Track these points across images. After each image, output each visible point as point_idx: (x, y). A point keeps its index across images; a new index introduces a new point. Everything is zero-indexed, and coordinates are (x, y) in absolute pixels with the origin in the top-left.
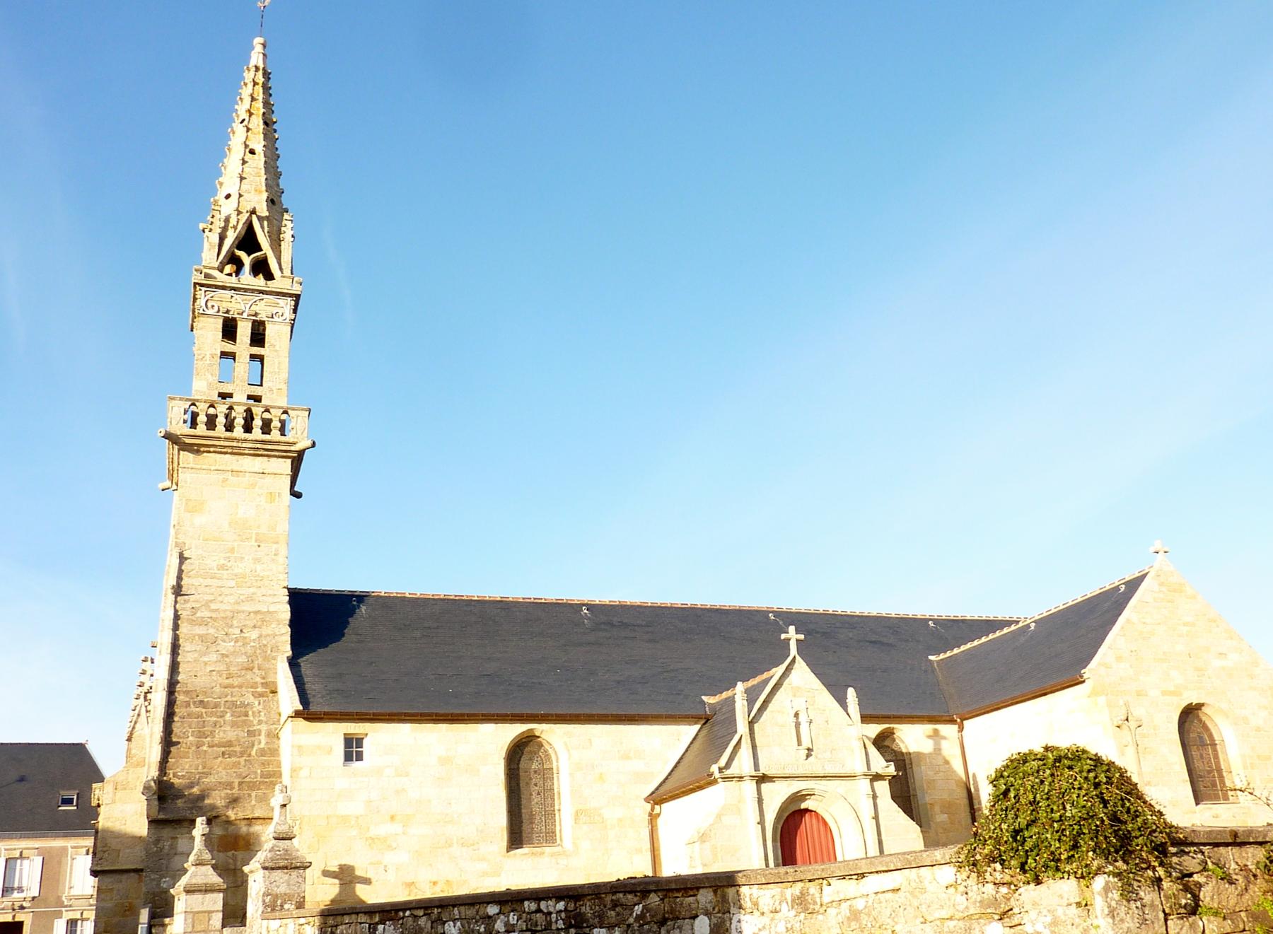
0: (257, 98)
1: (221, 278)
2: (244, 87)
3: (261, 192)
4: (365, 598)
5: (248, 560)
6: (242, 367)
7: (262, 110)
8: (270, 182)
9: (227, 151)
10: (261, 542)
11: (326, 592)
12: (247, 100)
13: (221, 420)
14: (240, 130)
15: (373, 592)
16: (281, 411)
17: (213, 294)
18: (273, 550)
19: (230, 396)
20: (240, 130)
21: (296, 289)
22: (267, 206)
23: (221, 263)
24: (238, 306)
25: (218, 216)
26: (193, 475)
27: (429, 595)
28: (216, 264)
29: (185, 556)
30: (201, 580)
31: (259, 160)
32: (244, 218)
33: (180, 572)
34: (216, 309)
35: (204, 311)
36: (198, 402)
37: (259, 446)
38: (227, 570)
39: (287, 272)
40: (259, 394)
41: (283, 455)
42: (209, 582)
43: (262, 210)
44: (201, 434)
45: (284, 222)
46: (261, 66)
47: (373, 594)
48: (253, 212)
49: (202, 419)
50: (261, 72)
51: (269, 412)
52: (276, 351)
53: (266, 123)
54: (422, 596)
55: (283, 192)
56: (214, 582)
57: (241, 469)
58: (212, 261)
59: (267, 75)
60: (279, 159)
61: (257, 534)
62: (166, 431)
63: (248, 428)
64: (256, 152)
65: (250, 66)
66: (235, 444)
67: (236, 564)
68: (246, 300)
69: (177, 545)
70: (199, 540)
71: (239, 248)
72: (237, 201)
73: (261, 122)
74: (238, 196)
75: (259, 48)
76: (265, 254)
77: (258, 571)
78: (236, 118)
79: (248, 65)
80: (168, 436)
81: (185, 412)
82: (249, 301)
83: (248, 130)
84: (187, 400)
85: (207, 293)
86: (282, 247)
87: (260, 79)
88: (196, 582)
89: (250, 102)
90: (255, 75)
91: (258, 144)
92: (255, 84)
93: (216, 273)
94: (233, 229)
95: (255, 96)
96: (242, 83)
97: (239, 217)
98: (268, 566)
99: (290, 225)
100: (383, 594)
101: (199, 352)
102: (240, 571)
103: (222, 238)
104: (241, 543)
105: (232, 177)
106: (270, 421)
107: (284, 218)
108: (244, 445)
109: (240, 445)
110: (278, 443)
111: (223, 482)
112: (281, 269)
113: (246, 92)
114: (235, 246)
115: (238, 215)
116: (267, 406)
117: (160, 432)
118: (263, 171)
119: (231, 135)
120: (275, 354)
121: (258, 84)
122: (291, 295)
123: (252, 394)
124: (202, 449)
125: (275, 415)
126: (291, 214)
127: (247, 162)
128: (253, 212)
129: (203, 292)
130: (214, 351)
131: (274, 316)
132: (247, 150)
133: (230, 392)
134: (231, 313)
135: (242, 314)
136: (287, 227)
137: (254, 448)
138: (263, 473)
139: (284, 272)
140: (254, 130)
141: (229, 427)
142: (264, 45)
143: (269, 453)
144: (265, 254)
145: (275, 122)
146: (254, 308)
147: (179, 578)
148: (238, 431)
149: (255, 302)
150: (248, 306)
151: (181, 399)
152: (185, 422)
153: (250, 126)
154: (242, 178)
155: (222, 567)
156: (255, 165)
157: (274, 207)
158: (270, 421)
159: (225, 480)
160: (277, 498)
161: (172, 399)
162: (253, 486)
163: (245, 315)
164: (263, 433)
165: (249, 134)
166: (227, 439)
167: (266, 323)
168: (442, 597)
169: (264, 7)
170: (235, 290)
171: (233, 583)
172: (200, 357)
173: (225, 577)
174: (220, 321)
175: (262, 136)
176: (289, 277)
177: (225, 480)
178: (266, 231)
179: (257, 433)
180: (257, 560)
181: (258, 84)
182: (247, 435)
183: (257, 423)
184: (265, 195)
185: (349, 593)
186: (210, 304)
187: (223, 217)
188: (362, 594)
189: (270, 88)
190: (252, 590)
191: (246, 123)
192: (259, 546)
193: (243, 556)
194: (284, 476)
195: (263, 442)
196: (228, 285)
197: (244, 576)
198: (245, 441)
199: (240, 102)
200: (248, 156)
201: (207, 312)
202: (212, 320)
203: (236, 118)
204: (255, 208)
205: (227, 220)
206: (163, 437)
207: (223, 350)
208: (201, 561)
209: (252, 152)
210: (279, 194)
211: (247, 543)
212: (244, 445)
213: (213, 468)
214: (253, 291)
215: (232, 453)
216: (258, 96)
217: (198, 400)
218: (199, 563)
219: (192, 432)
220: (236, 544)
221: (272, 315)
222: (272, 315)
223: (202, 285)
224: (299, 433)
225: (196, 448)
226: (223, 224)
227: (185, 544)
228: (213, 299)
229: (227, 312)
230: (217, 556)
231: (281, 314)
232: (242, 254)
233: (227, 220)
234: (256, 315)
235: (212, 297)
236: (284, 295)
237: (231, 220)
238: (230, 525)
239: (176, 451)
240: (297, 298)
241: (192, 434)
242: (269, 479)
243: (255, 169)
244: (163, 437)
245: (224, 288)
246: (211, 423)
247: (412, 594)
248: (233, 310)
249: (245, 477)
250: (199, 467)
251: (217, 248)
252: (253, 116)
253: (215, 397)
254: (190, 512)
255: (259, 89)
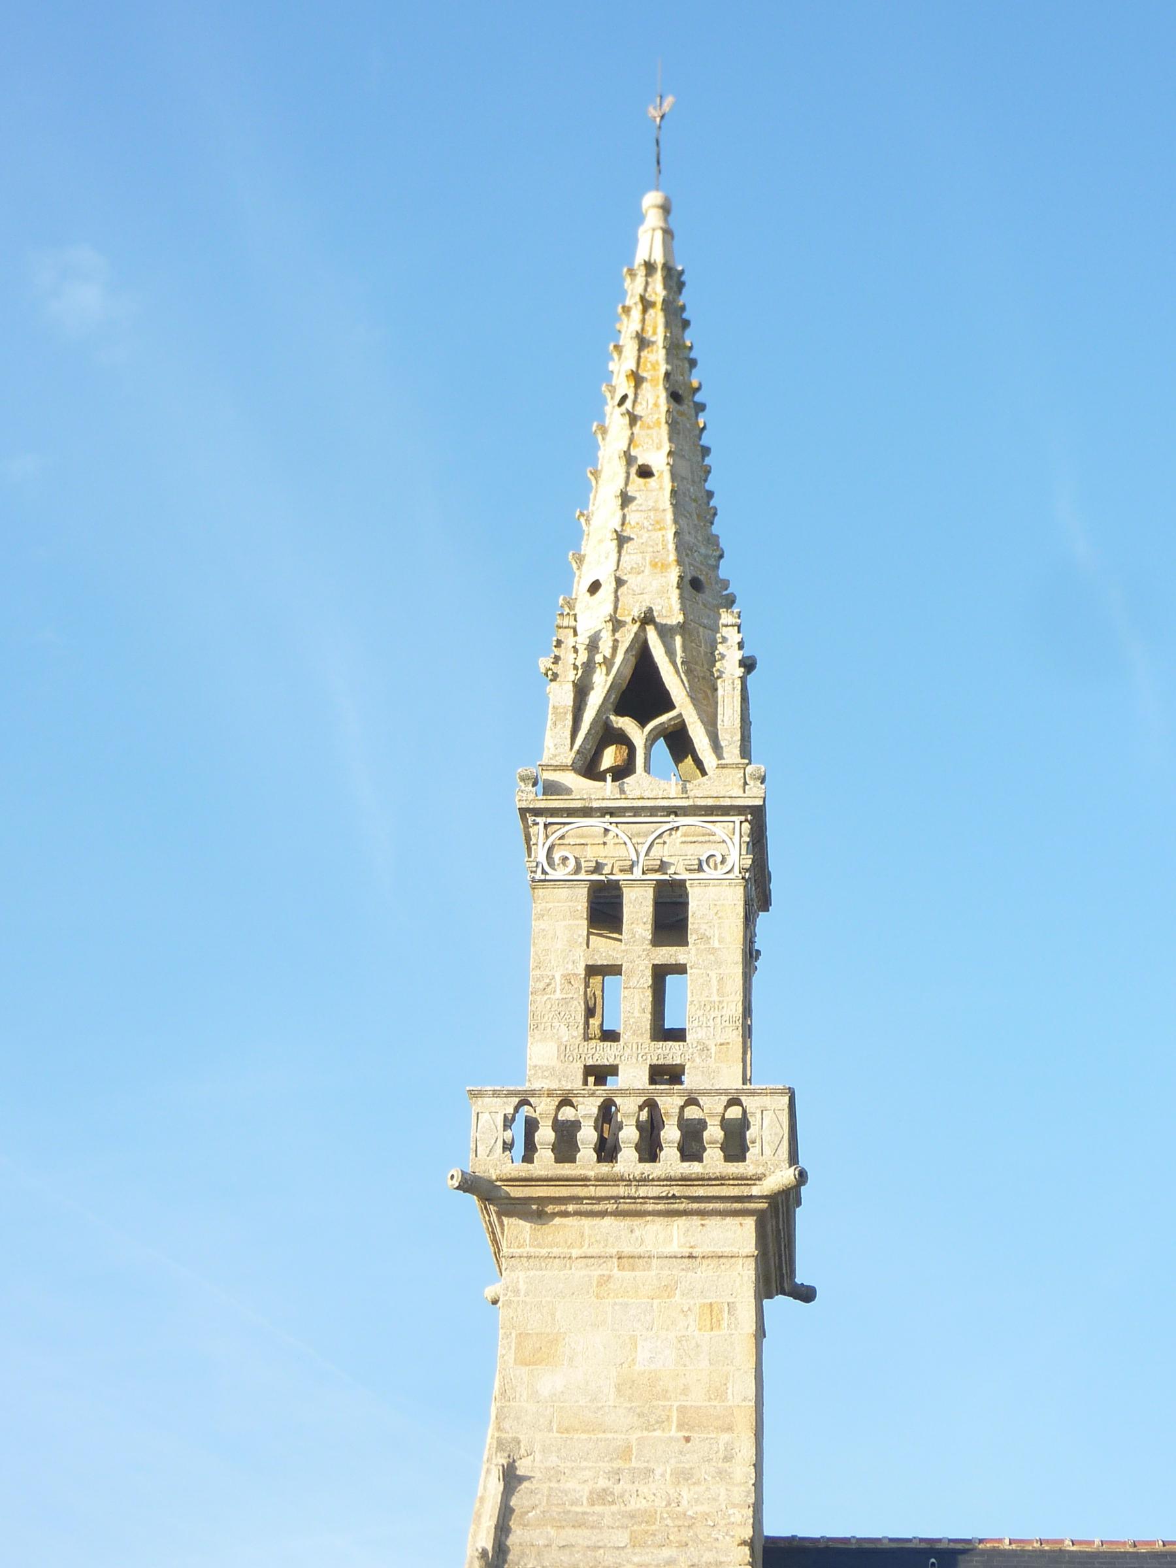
0: (653, 339)
1: (583, 789)
2: (624, 317)
3: (665, 567)
4: (960, 1557)
5: (663, 1475)
6: (636, 1001)
7: (663, 368)
8: (687, 538)
9: (592, 478)
10: (691, 1429)
11: (866, 1546)
12: (630, 347)
13: (587, 1135)
14: (616, 420)
15: (981, 1541)
16: (724, 1099)
17: (568, 827)
18: (722, 1448)
19: (613, 1070)
20: (616, 420)
21: (753, 796)
22: (681, 597)
23: (578, 752)
24: (622, 852)
25: (570, 641)
26: (531, 1273)
27: (1124, 1543)
28: (568, 757)
29: (518, 1473)
30: (553, 1532)
31: (661, 487)
32: (627, 636)
33: (505, 1514)
34: (572, 863)
35: (544, 872)
36: (533, 1095)
37: (676, 1191)
38: (613, 1503)
39: (732, 753)
40: (678, 1061)
41: (735, 1207)
42: (570, 1535)
43: (671, 610)
44: (543, 1173)
45: (724, 631)
46: (658, 258)
47: (981, 1546)
48: (647, 619)
49: (545, 1134)
50: (659, 276)
51: (699, 1105)
52: (712, 951)
53: (675, 396)
54: (1105, 1548)
55: (721, 556)
56: (581, 1537)
57: (641, 1250)
58: (561, 750)
59: (674, 280)
60: (710, 477)
61: (682, 1410)
62: (463, 1173)
63: (649, 1149)
64: (654, 470)
65: (636, 267)
66: (621, 1191)
67: (634, 1488)
68: (638, 835)
69: (501, 1445)
70: (550, 1430)
71: (620, 712)
72: (612, 597)
73: (663, 395)
74: (614, 584)
75: (653, 219)
76: (680, 715)
77: (684, 1503)
78: (608, 395)
79: (632, 263)
80: (470, 1185)
81: (508, 1123)
82: (646, 835)
83: (633, 419)
84: (511, 1094)
85: (551, 829)
86: (720, 692)
87: (658, 291)
88: (538, 1536)
89: (636, 353)
90: (647, 283)
91: (656, 452)
92: (646, 305)
93: (571, 780)
94: (604, 668)
95: (648, 335)
96: (620, 310)
97: (617, 635)
98: (708, 1489)
99: (734, 637)
100: (1006, 1545)
101: (538, 972)
102: (642, 1504)
103: (581, 691)
104: (645, 1433)
105: (601, 541)
106: (575, 1125)
107: (723, 621)
108: (642, 1191)
109: (632, 1191)
110: (721, 1180)
111: (599, 1285)
112: (717, 747)
113: (630, 326)
114: (610, 706)
115: (614, 631)
116: (691, 1092)
117: (452, 1177)
118: (669, 516)
119: (600, 437)
120: (712, 957)
121: (652, 305)
122: (740, 810)
123: (660, 1062)
124: (550, 1209)
125: (711, 1109)
126: (736, 610)
127: (632, 499)
128: (647, 619)
129: (541, 826)
130: (570, 966)
131: (705, 866)
132: (633, 470)
133: (611, 1061)
134: (607, 870)
135: (630, 870)
136: (729, 643)
137: (667, 1198)
138: (691, 1257)
139: (725, 755)
140: (648, 420)
141: (607, 1150)
142: (666, 209)
143: (702, 1206)
144: (680, 715)
145: (698, 389)
146: (656, 852)
147: (502, 1529)
148: (628, 1161)
149: (660, 836)
150: (643, 850)
151: (496, 1094)
152: (508, 1146)
153: (638, 411)
154: (622, 540)
155: (601, 1497)
156: (651, 504)
157: (700, 597)
158: (702, 1125)
159: (604, 1281)
160: (726, 1315)
161: (476, 1094)
162: (668, 1290)
163: (637, 873)
164: (557, 1161)
165: (636, 429)
166: (602, 1180)
167: (688, 883)
168: (1159, 1547)
169: (662, 117)
170: (612, 815)
171: (622, 1538)
172: (541, 985)
173: (607, 1521)
174: (583, 893)
175: (664, 430)
176: (737, 766)
177: (604, 1281)
178: (679, 661)
179: (670, 1161)
180: (684, 1476)
181: (652, 305)
182: (648, 1168)
183: (671, 1134)
184: (674, 574)
185: (923, 1545)
186: (557, 856)
187: (583, 639)
188: (952, 1545)
189: (683, 308)
190: (666, 1553)
191: (628, 404)
192: (688, 1439)
193: (652, 1465)
194: (740, 1261)
195: (685, 1180)
196: (595, 804)
197: (648, 1517)
198: (644, 1180)
199: (615, 355)
200: (637, 482)
201: (553, 875)
202: (563, 893)
203: (608, 395)
204: (650, 610)
205: (593, 646)
206: (458, 1188)
207: (590, 963)
208: (554, 1485)
209: (645, 472)
210: (712, 562)
211: (658, 1433)
212: (642, 1191)
213: (575, 1252)
214: (653, 811)
215: (616, 1214)
216: (655, 333)
217: (533, 1093)
218: (550, 1488)
219: (522, 1169)
220: (634, 1436)
221: (700, 865)
222: (700, 865)
223: (538, 812)
224: (768, 1151)
225: (534, 1207)
226: (583, 657)
227: (519, 1443)
228: (565, 841)
229: (598, 868)
230: (590, 1468)
231: (719, 859)
232: (626, 724)
233: (593, 646)
234: (663, 867)
235: (562, 838)
236: (726, 810)
237: (601, 644)
238: (619, 1391)
239: (494, 1218)
240: (757, 816)
241: (523, 1174)
242: (705, 1272)
243: (652, 514)
244: (458, 1188)
245: (587, 812)
246: (566, 1147)
247: (1081, 1543)
248: (609, 862)
249: (649, 1269)
250: (544, 1252)
251: (570, 717)
252: (645, 385)
253: (574, 1081)
254: (527, 1365)
255: (657, 317)
